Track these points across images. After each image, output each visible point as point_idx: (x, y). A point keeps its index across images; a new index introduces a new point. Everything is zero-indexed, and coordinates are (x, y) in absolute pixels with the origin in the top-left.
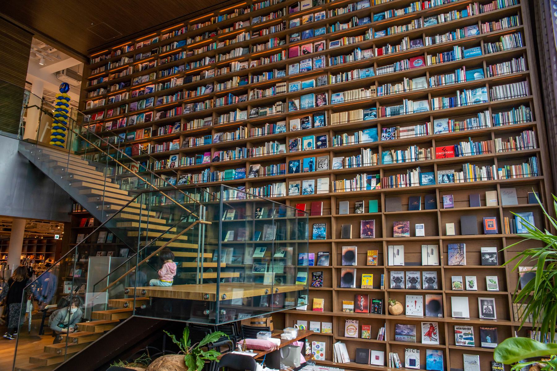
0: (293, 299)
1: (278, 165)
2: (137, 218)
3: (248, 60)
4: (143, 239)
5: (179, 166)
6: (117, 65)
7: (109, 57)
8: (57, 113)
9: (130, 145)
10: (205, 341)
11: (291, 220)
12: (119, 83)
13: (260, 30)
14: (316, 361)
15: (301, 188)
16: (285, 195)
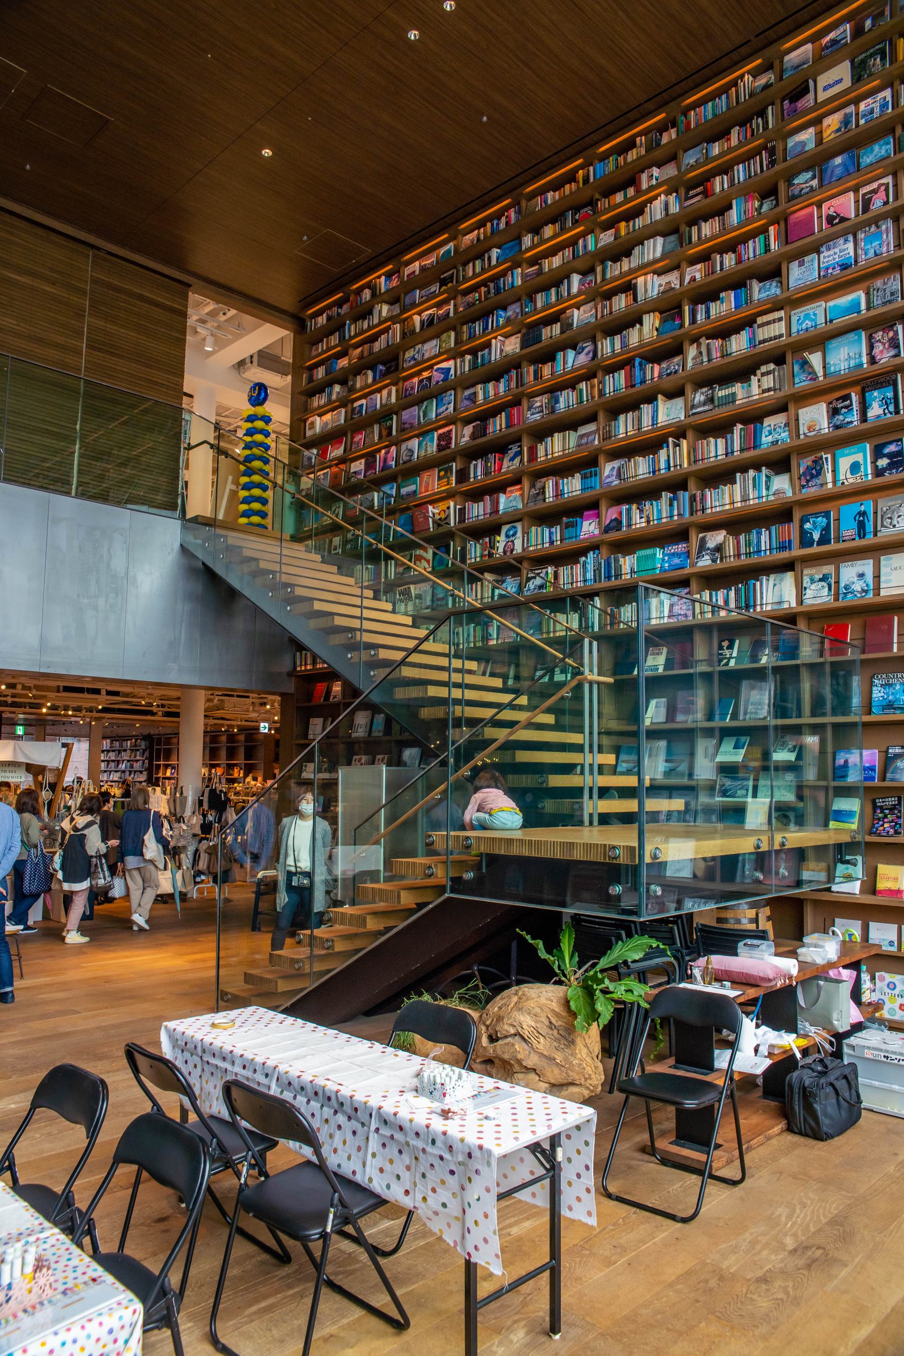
0: (823, 865)
1: (773, 528)
2: (443, 676)
3: (677, 267)
4: (458, 723)
5: (524, 549)
6: (365, 326)
7: (346, 308)
8: (248, 452)
9: (407, 509)
10: (612, 957)
11: (813, 667)
12: (372, 367)
13: (705, 180)
14: (889, 1021)
15: (837, 582)
16: (794, 604)
